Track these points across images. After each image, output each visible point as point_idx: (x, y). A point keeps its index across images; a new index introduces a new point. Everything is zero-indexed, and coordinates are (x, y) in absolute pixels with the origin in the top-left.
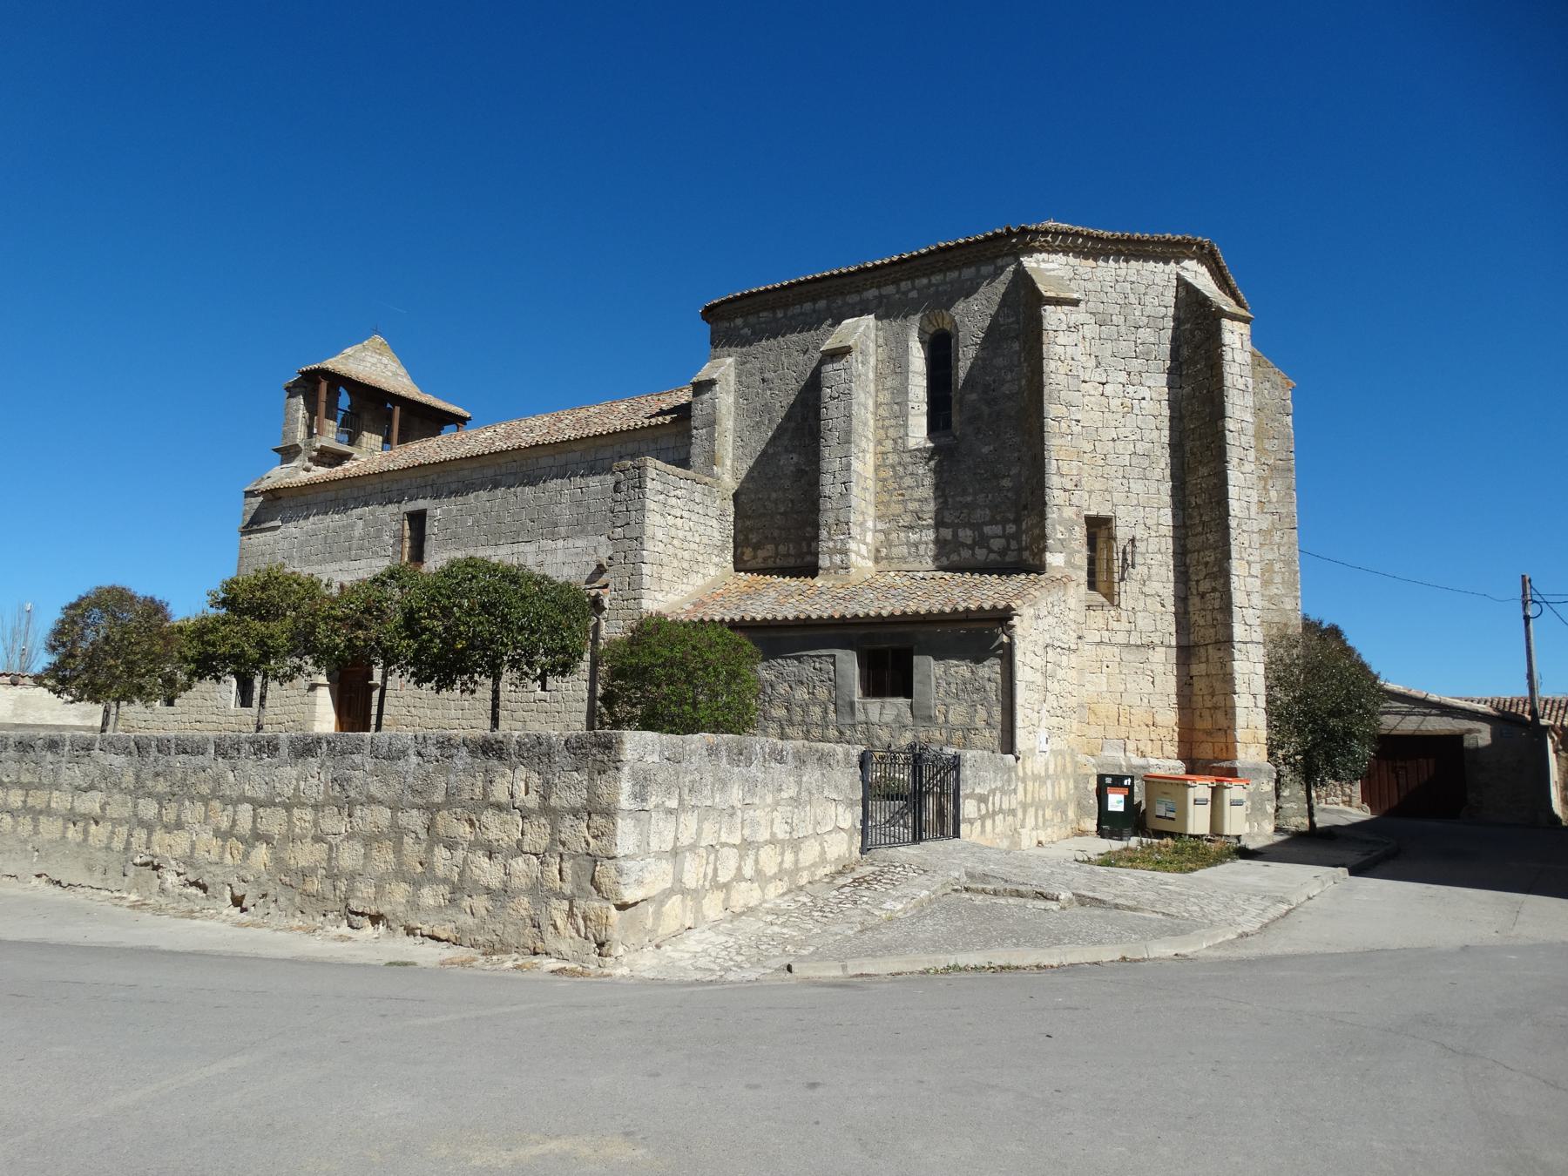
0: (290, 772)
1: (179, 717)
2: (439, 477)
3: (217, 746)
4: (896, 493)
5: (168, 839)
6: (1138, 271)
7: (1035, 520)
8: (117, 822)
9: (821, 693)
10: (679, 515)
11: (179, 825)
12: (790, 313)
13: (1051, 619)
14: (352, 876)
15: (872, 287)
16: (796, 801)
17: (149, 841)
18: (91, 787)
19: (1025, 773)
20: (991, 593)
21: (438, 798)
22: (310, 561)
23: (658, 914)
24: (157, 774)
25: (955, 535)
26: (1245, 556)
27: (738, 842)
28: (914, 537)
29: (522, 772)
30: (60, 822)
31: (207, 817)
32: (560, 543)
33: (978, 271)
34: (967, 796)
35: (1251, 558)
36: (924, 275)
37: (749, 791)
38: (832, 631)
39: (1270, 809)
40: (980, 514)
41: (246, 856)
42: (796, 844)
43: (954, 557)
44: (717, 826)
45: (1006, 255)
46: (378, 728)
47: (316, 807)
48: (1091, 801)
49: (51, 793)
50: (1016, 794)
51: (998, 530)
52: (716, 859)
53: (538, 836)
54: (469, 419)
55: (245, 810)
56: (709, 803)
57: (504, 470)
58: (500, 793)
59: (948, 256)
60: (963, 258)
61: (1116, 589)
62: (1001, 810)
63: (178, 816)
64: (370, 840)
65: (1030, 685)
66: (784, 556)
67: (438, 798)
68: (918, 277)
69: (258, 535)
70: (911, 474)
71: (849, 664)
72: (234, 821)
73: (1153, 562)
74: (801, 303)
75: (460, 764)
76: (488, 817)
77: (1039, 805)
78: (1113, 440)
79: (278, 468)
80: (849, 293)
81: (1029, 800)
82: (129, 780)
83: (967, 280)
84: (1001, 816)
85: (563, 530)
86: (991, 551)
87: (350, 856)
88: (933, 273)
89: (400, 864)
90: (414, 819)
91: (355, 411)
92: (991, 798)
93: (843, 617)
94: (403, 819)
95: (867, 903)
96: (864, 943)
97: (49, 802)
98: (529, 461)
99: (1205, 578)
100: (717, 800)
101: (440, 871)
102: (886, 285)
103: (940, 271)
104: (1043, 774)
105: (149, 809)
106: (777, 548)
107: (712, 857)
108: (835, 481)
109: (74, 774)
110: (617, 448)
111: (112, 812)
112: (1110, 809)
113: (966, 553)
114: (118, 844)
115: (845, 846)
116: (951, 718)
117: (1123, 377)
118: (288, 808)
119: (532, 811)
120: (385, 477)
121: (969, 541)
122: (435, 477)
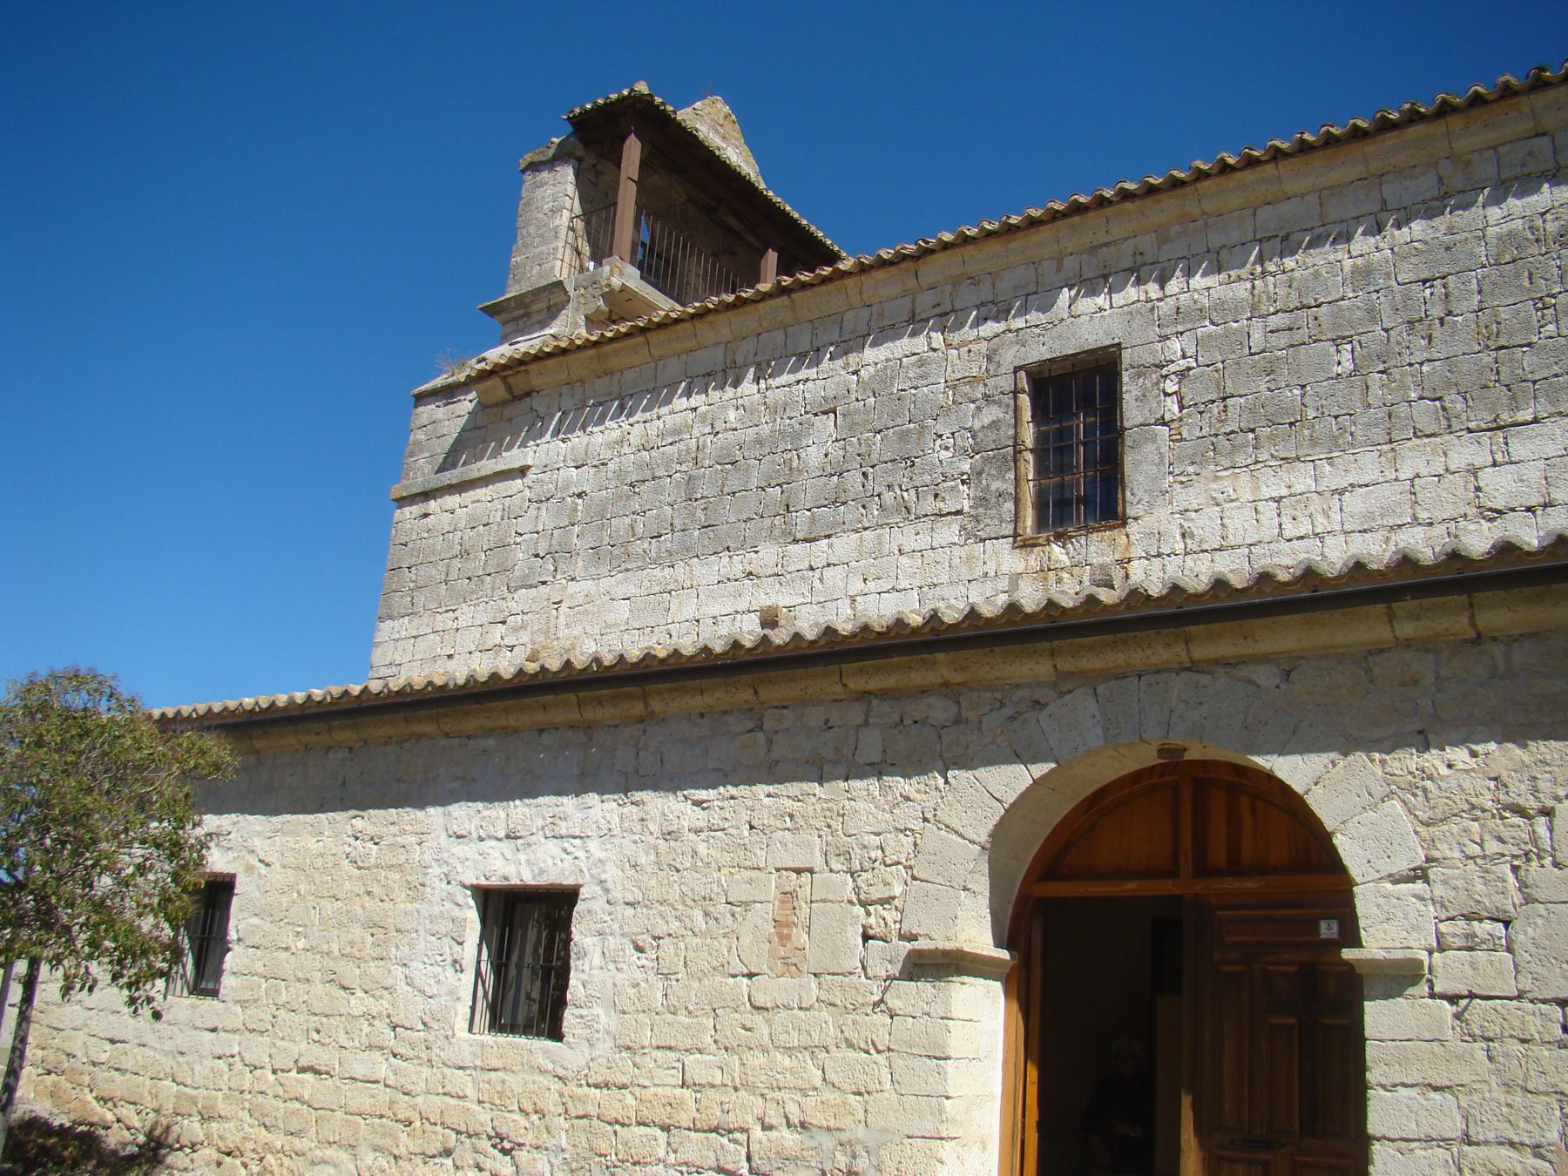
1: (234, 1045)
7: (563, 936)
39: (478, 1063)
69: (451, 501)
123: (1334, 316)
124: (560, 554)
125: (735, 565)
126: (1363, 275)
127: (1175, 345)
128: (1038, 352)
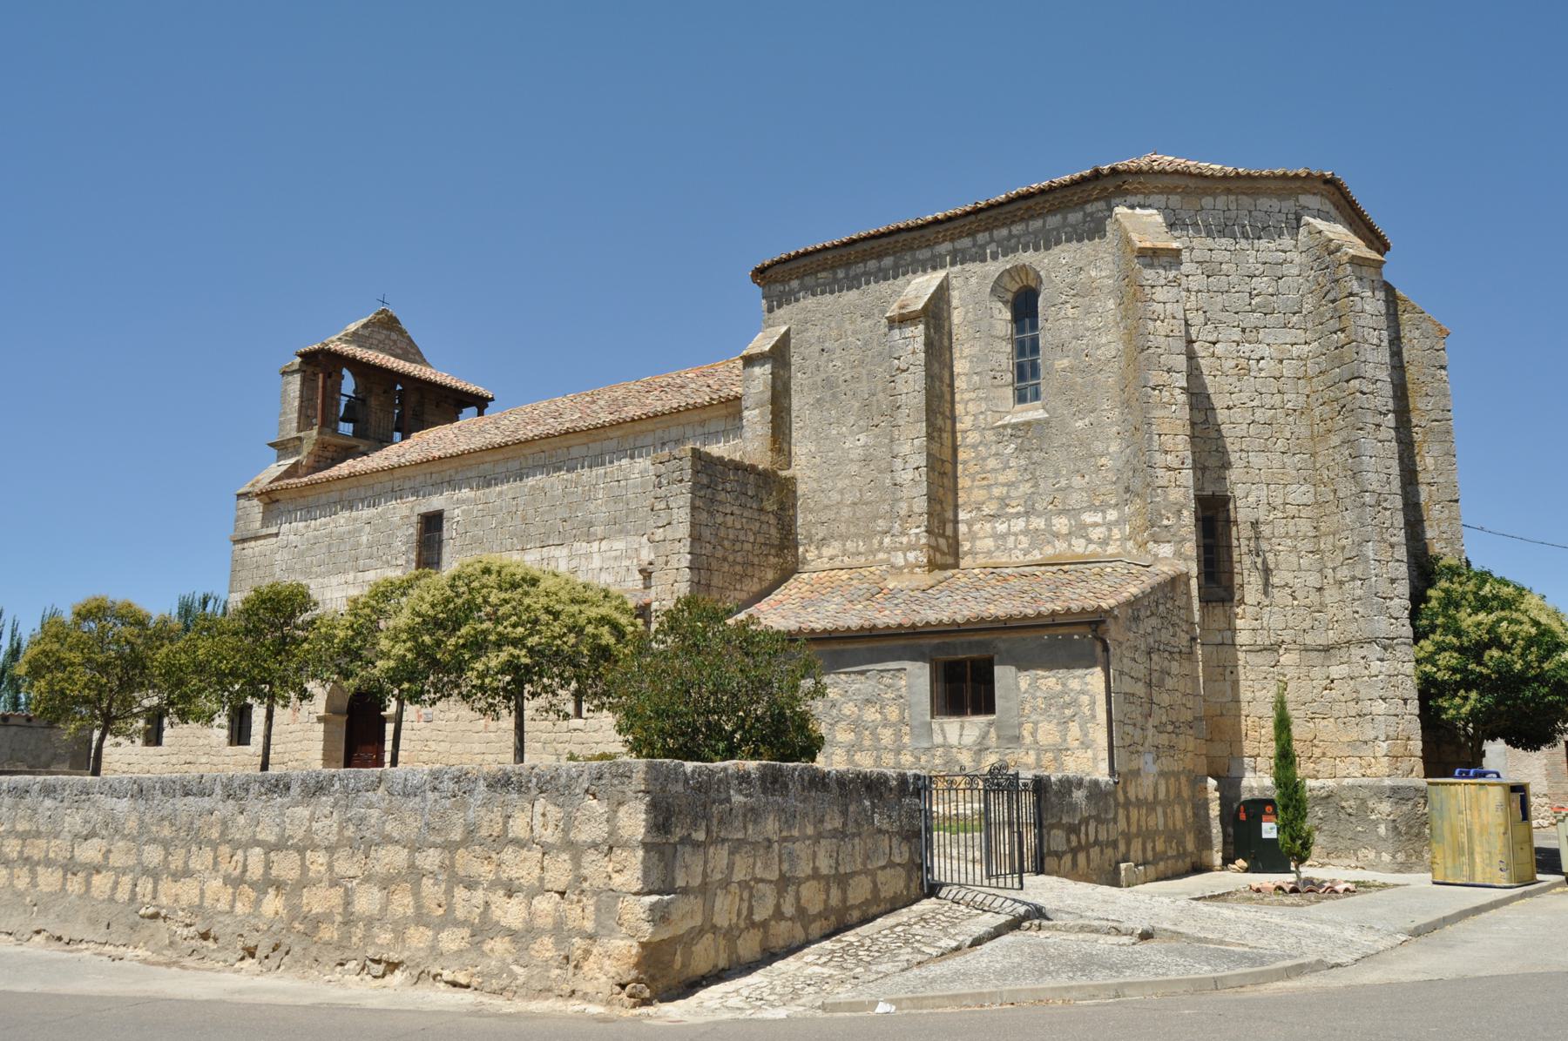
0: (303, 812)
2: (457, 473)
3: (225, 786)
4: (978, 477)
5: (176, 888)
6: (1250, 212)
8: (124, 871)
9: (893, 713)
10: (728, 511)
11: (187, 873)
12: (852, 273)
13: (1154, 621)
14: (370, 922)
15: (944, 241)
16: (840, 834)
17: (155, 890)
18: (92, 834)
19: (1126, 798)
20: (1085, 591)
21: (456, 835)
22: (311, 573)
23: (688, 954)
24: (163, 819)
26: (1386, 536)
27: (775, 876)
28: (1002, 528)
29: (540, 804)
30: (60, 873)
31: (216, 863)
32: (595, 545)
33: (1065, 219)
34: (1052, 826)
35: (1394, 539)
36: (1004, 225)
37: (787, 821)
38: (902, 642)
40: (1075, 499)
41: (258, 903)
42: (842, 880)
43: (1049, 550)
44: (751, 860)
45: (1097, 199)
46: (394, 762)
47: (331, 849)
49: (49, 842)
50: (1116, 823)
51: (1098, 518)
52: (751, 896)
53: (559, 871)
54: (492, 399)
55: (256, 855)
56: (740, 835)
57: (530, 462)
58: (518, 828)
59: (1031, 202)
60: (1047, 205)
62: (1096, 842)
63: (186, 863)
64: (387, 883)
65: (1000, 697)
66: (853, 554)
67: (456, 835)
68: (997, 227)
69: (253, 544)
71: (916, 678)
72: (245, 866)
73: (1280, 548)
74: (864, 261)
76: (508, 854)
77: (1148, 835)
79: (274, 465)
80: (920, 247)
81: (1134, 829)
82: (132, 825)
83: (1053, 229)
84: (1097, 849)
85: (599, 530)
86: (1090, 541)
87: (367, 901)
88: (1013, 222)
89: (419, 906)
90: (430, 859)
91: (360, 396)
92: (1083, 829)
93: (914, 626)
95: (919, 941)
96: (908, 979)
97: (48, 851)
98: (560, 451)
100: (750, 831)
101: (460, 914)
102: (960, 237)
103: (1022, 219)
104: (1151, 798)
105: (153, 855)
106: (844, 545)
107: (746, 895)
108: (907, 466)
110: (659, 433)
111: (117, 860)
113: (1061, 546)
114: (123, 895)
115: (902, 884)
116: (1040, 737)
117: (1236, 335)
118: (301, 851)
119: (552, 846)
120: (397, 473)
121: (1065, 530)
122: (452, 472)
125: (342, 578)
126: (500, 493)
127: (456, 511)
128: (424, 510)
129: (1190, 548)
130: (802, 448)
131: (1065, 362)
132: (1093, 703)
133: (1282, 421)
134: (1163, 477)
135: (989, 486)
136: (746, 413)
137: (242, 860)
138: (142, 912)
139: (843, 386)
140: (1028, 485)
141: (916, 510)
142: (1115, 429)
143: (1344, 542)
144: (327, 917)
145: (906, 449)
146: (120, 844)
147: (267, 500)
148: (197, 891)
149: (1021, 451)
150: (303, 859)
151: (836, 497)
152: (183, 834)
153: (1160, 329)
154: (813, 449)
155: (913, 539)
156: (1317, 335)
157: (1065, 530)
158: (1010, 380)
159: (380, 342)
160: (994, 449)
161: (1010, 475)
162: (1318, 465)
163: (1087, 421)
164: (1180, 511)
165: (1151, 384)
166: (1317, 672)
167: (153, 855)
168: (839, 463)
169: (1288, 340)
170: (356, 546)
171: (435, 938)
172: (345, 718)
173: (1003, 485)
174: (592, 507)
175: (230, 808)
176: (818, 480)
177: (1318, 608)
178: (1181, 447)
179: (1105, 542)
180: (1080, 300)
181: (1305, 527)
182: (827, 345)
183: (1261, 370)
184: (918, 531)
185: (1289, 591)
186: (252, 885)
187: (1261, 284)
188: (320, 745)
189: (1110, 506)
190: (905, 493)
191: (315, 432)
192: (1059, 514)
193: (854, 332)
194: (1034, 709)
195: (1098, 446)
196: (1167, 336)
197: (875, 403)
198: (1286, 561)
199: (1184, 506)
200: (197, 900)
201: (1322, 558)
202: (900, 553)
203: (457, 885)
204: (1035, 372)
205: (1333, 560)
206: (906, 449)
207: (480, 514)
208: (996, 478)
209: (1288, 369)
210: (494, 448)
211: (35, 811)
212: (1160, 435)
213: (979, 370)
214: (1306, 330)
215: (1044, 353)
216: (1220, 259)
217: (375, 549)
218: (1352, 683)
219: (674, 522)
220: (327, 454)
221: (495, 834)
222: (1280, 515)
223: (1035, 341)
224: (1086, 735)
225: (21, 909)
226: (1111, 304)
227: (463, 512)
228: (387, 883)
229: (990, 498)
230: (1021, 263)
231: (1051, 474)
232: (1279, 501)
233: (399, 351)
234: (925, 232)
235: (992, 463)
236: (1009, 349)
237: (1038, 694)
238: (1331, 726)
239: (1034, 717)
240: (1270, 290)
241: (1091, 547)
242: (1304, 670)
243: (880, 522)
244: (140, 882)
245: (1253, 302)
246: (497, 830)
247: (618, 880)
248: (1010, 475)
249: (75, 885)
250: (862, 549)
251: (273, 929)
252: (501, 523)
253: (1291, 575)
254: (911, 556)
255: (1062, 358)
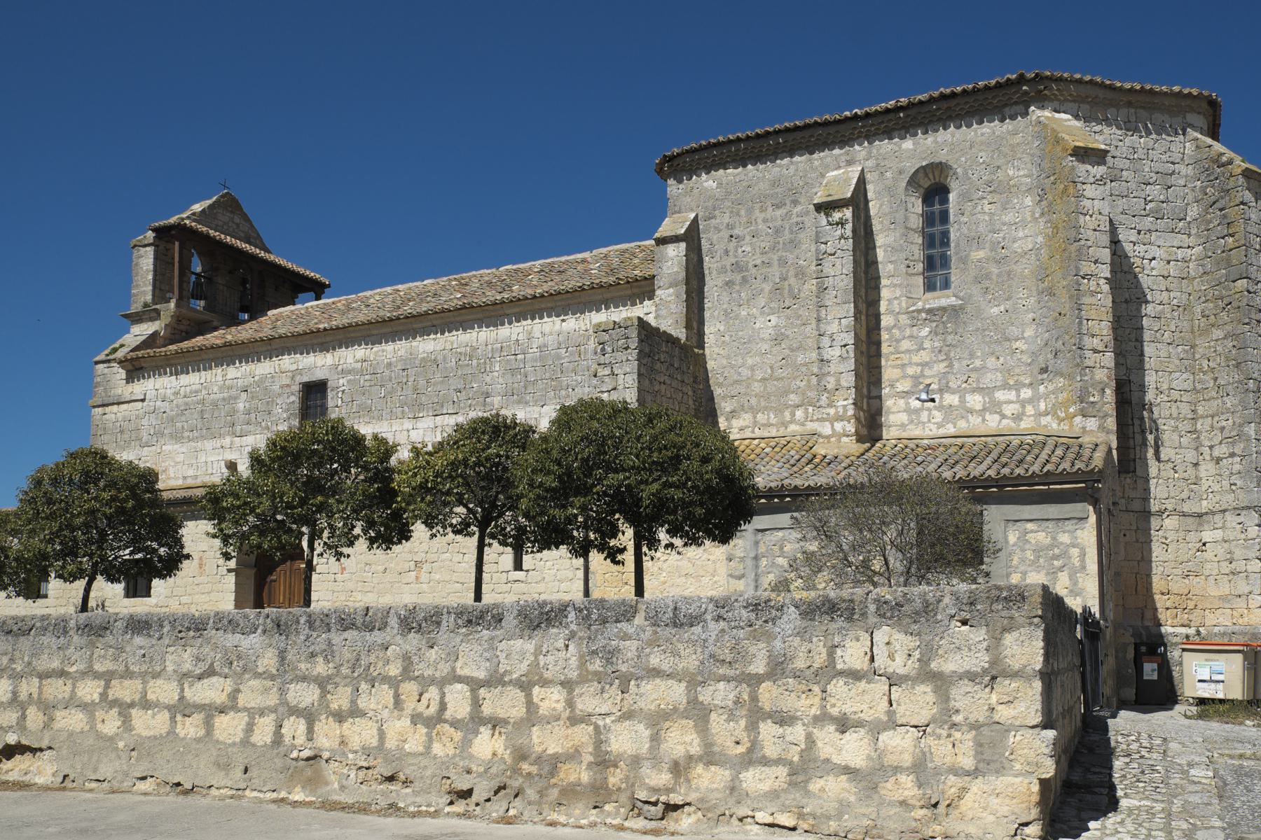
4: (893, 357)
8: (254, 713)
11: (356, 712)
18: (210, 672)
21: (759, 667)
25: (962, 400)
30: (166, 715)
40: (989, 379)
41: (466, 743)
43: (962, 424)
45: (1016, 103)
48: (1130, 671)
51: (1012, 395)
54: (329, 286)
59: (952, 103)
61: (1132, 456)
63: (354, 702)
66: (764, 425)
67: (759, 667)
69: (115, 408)
70: (911, 336)
73: (1165, 428)
75: (789, 628)
76: (838, 687)
78: (1126, 302)
82: (268, 661)
86: (1004, 416)
94: (705, 695)
99: (1221, 443)
105: (304, 695)
106: (755, 417)
109: (182, 658)
112: (1145, 678)
113: (975, 420)
118: (525, 686)
123: (382, 378)
124: (159, 434)
125: (217, 443)
127: (341, 381)
129: (1111, 423)
130: (712, 329)
131: (981, 254)
132: (1083, 555)
133: (1168, 316)
134: (1091, 358)
135: (903, 366)
136: (658, 292)
137: (438, 698)
138: (295, 754)
139: (754, 271)
140: (945, 364)
141: (844, 384)
142: (1031, 316)
143: (1224, 423)
144: (573, 756)
145: (833, 328)
146: (252, 683)
147: (131, 367)
148: (375, 732)
149: (936, 334)
150: (529, 696)
151: (745, 372)
152: (345, 670)
153: (1089, 223)
154: (722, 328)
155: (841, 410)
156: (1202, 240)
157: (979, 407)
158: (921, 270)
159: (225, 223)
160: (908, 332)
161: (924, 356)
162: (1197, 356)
163: (1002, 308)
164: (1103, 390)
165: (1081, 273)
166: (1192, 536)
167: (304, 695)
168: (749, 342)
169: (1175, 244)
170: (233, 412)
171: (736, 778)
172: (253, 571)
173: (918, 365)
174: (488, 379)
175: (415, 642)
176: (728, 357)
177: (1193, 481)
178: (1105, 332)
179: (1018, 418)
180: (998, 196)
181: (1185, 409)
182: (736, 232)
183: (1153, 269)
184: (845, 403)
185: (1172, 465)
186: (455, 724)
187: (1154, 191)
188: (233, 597)
189: (1024, 385)
190: (833, 368)
191: (172, 305)
192: (974, 392)
193: (765, 221)
194: (1023, 560)
195: (1014, 331)
196: (1095, 230)
197: (787, 287)
198: (1170, 439)
199: (1107, 385)
200: (374, 742)
201: (1198, 438)
202: (827, 423)
203: (764, 720)
204: (945, 262)
205: (1211, 439)
206: (833, 328)
207: (367, 384)
208: (910, 358)
209: (1173, 269)
210: (384, 321)
211: (122, 650)
212: (1088, 320)
213: (893, 259)
214: (1189, 235)
215: (958, 245)
216: (1121, 166)
217: (253, 416)
218: (1226, 545)
219: (620, 387)
220: (182, 327)
221: (816, 665)
222: (1166, 399)
223: (945, 234)
224: (1075, 584)
225: (113, 755)
226: (1028, 201)
227: (349, 381)
228: (658, 720)
229: (904, 377)
230: (937, 161)
231: (966, 355)
232: (1165, 386)
233: (242, 235)
234: (841, 127)
235: (905, 345)
236: (920, 241)
237: (1027, 546)
238: (1202, 582)
239: (1022, 568)
240: (1162, 197)
241: (1005, 422)
242: (1182, 534)
243: (792, 396)
244: (286, 723)
245: (1148, 207)
246: (820, 659)
247: (1004, 714)
248: (924, 356)
249: (190, 728)
250: (773, 420)
251: (491, 771)
252: (390, 393)
253: (1173, 451)
254: (838, 426)
255: (978, 249)
